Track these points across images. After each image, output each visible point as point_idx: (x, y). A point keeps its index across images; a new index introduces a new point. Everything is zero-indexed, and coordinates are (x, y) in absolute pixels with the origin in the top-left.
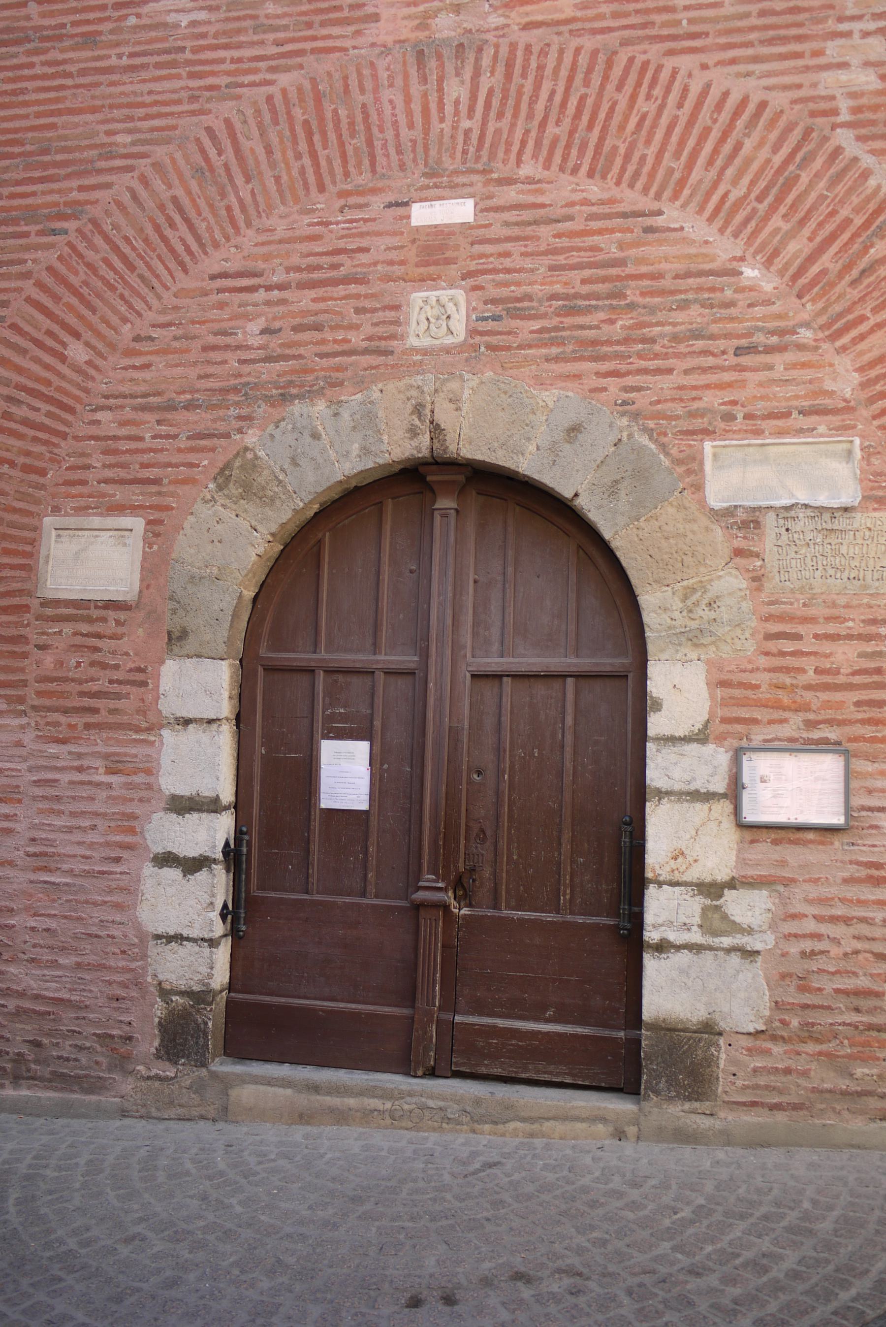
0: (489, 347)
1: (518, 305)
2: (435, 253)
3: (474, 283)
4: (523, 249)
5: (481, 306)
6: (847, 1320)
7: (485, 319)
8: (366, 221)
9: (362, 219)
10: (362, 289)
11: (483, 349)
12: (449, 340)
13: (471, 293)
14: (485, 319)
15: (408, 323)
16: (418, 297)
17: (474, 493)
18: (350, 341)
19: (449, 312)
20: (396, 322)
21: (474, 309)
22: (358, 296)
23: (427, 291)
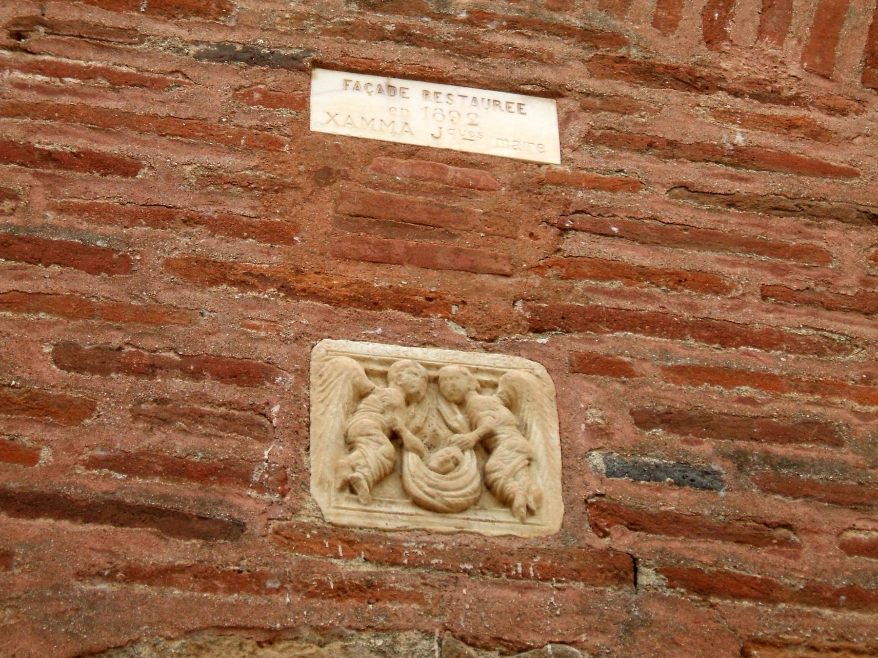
0: (674, 575)
1: (778, 449)
2: (411, 238)
3: (583, 348)
4: (770, 279)
5: (625, 430)
6: (91, 60)
7: (653, 474)
8: (118, 82)
9: (106, 73)
10: (97, 287)
11: (648, 577)
12: (493, 525)
13: (579, 380)
14: (653, 474)
15: (300, 431)
16: (340, 357)
17: (80, 521)
18: (31, 458)
19: (486, 423)
20: (254, 424)
21: (598, 432)
22: (77, 308)
23: (383, 339)
